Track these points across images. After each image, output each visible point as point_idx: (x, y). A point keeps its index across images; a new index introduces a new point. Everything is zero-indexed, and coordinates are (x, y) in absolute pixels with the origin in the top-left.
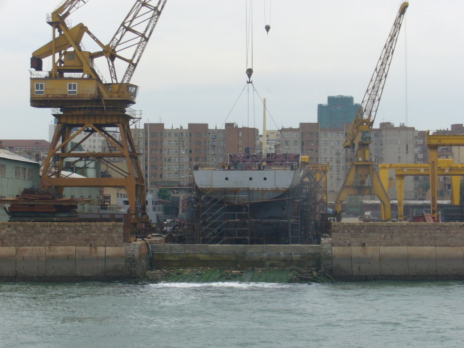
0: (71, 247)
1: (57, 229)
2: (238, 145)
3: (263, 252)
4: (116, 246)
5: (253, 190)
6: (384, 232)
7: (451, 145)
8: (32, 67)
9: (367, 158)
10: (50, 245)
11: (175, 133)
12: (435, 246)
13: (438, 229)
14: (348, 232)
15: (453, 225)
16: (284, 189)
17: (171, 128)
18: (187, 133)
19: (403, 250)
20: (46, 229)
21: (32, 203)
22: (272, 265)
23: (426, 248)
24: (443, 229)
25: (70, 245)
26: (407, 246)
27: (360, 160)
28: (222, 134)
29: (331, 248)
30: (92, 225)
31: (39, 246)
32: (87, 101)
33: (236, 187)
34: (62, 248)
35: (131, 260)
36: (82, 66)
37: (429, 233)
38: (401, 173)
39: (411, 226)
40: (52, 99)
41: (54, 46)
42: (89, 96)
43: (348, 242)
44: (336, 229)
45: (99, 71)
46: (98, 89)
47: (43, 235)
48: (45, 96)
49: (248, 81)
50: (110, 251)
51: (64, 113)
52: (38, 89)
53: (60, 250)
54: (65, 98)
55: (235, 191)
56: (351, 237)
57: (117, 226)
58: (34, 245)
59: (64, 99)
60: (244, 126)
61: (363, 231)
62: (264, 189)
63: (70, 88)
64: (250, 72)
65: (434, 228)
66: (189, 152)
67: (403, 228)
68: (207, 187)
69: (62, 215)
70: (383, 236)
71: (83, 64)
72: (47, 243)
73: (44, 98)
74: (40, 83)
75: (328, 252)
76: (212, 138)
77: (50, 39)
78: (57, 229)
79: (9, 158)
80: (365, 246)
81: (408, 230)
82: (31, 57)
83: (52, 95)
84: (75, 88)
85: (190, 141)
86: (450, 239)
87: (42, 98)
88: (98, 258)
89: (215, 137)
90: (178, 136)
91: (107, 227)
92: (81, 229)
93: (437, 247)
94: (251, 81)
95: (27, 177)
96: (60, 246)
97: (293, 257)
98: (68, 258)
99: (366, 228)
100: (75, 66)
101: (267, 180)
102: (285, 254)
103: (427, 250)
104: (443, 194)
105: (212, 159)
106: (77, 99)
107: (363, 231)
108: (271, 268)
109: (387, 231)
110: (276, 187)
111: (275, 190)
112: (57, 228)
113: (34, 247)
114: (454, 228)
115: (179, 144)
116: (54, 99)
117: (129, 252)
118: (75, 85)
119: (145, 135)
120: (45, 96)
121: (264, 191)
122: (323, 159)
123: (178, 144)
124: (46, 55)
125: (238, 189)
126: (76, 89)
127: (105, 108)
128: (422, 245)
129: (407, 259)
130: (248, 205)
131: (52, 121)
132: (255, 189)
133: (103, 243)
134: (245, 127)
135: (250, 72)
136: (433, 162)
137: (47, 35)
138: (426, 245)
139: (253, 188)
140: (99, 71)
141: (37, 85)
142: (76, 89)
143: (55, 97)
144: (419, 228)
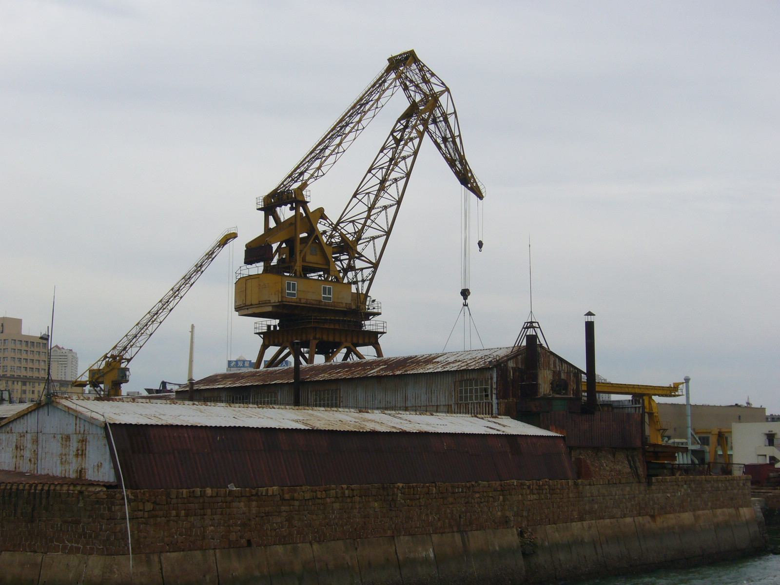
48: (298, 300)
51: (278, 330)
54: (319, 305)
64: (465, 293)
83: (305, 300)
100: (317, 264)
104: (42, 338)
120: (298, 300)
135: (465, 293)
143: (308, 303)
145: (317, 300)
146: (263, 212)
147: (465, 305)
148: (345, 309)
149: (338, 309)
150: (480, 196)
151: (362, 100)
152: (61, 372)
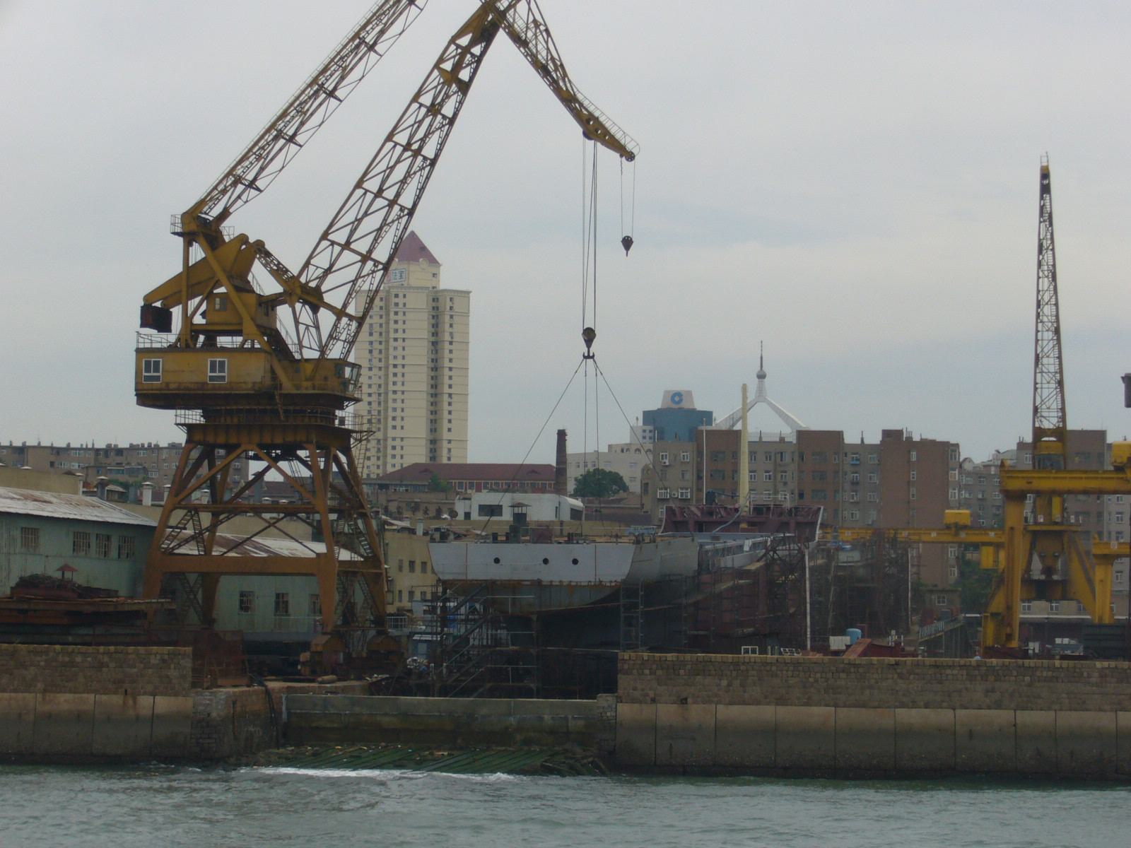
0: (85, 695)
1: (60, 658)
2: (909, 482)
3: (510, 715)
4: (176, 695)
5: (551, 586)
6: (726, 675)
7: (1100, 493)
8: (143, 325)
9: (1057, 515)
10: (45, 691)
11: (766, 453)
12: (836, 706)
13: (843, 671)
14: (651, 674)
15: (876, 662)
16: (613, 584)
17: (859, 442)
18: (793, 453)
19: (767, 713)
20: (38, 658)
21: (25, 606)
22: (527, 742)
23: (816, 710)
24: (852, 670)
25: (84, 693)
26: (777, 704)
27: (1042, 520)
28: (875, 455)
29: (614, 706)
30: (129, 651)
31: (22, 692)
32: (247, 396)
33: (516, 577)
34: (69, 696)
35: (203, 724)
36: (241, 324)
37: (823, 680)
38: (1106, 551)
39: (785, 663)
40: (177, 392)
41: (184, 283)
42: (250, 386)
43: (651, 694)
44: (626, 667)
45: (287, 332)
46: (273, 371)
47: (32, 670)
49: (586, 354)
50: (164, 704)
52: (215, 372)
53: (65, 701)
55: (514, 586)
56: (658, 685)
57: (179, 654)
58: (15, 691)
59: (201, 392)
60: (924, 437)
61: (682, 672)
62: (573, 584)
63: (213, 370)
64: (589, 335)
65: (833, 669)
66: (797, 497)
67: (768, 668)
68: (456, 578)
69: (83, 631)
70: (724, 683)
71: (242, 319)
72: (40, 686)
73: (160, 390)
74: (218, 360)
75: (609, 714)
76: (852, 465)
77: (177, 268)
78: (60, 658)
79: (45, 514)
80: (686, 703)
81: (779, 672)
82: (142, 304)
83: (177, 384)
84: (222, 370)
85: (801, 471)
86: (867, 692)
87: (157, 390)
88: (138, 718)
89: (858, 463)
90: (773, 458)
91: (158, 657)
92: (106, 659)
93: (838, 709)
94: (591, 355)
95: (114, 553)
96: (65, 693)
97: (570, 725)
98: (79, 717)
99: (689, 667)
101: (493, 563)
102: (553, 718)
103: (818, 714)
105: (852, 514)
106: (227, 392)
107: (682, 672)
108: (526, 748)
109: (734, 673)
110: (597, 580)
111: (595, 585)
112: (60, 657)
113: (13, 695)
114: (877, 669)
115: (775, 477)
116: (181, 392)
117: (201, 708)
118: (222, 364)
119: (698, 457)
121: (572, 588)
122: (1114, 516)
123: (772, 478)
124: (180, 299)
125: (519, 582)
126: (159, 372)
127: (281, 411)
128: (807, 704)
129: (774, 731)
130: (534, 618)
131: (637, 419)
132: (554, 583)
133: (150, 688)
134: (926, 439)
135: (589, 335)
136: (1012, 528)
137: (167, 259)
138: (818, 704)
139: (551, 582)
140: (287, 332)
141: (148, 363)
142: (159, 372)
144: (801, 668)
145: (197, 383)
146: (879, 443)
147: (588, 357)
148: (252, 392)
149: (237, 392)
150: (630, 157)
151: (326, 72)
152: (370, 395)
